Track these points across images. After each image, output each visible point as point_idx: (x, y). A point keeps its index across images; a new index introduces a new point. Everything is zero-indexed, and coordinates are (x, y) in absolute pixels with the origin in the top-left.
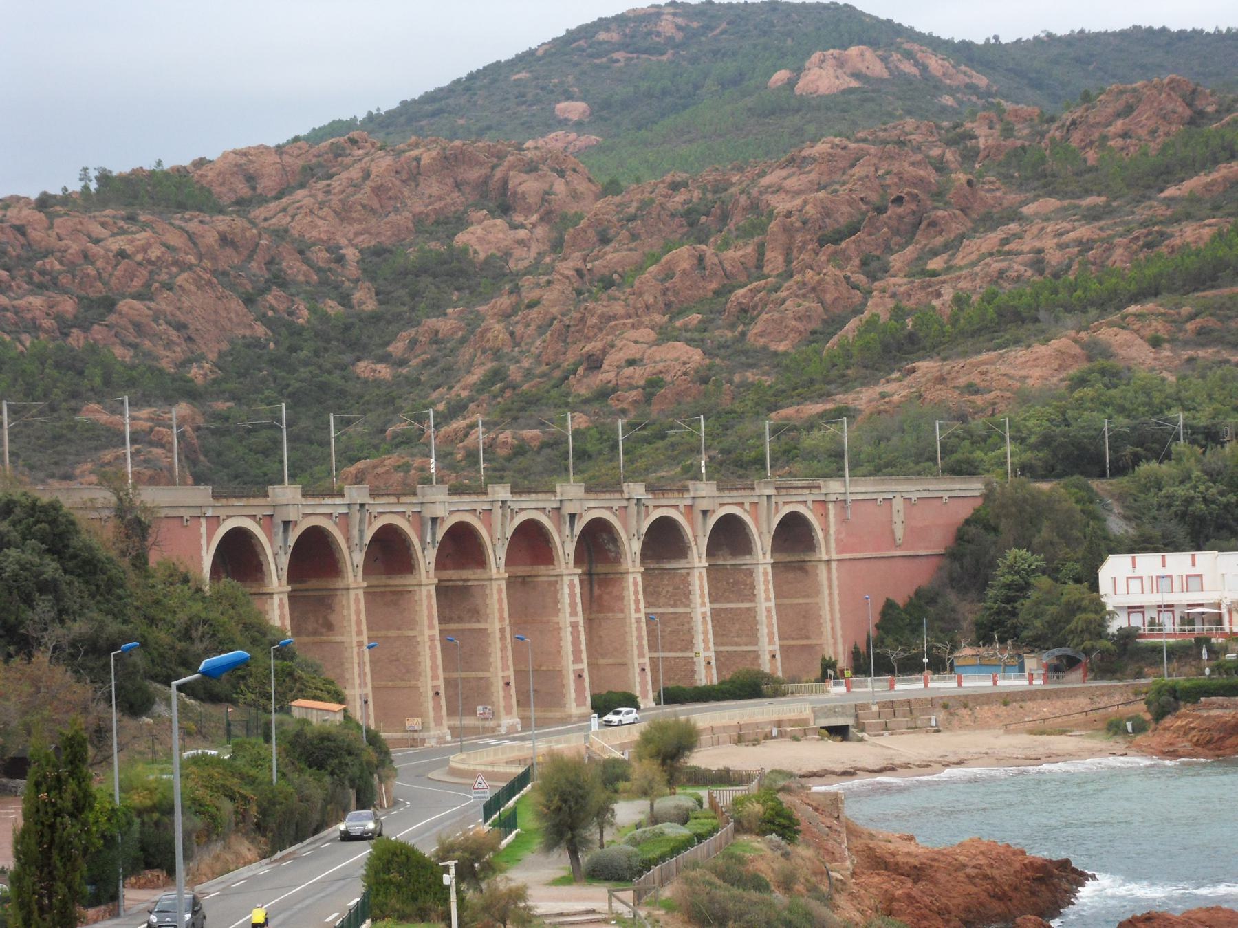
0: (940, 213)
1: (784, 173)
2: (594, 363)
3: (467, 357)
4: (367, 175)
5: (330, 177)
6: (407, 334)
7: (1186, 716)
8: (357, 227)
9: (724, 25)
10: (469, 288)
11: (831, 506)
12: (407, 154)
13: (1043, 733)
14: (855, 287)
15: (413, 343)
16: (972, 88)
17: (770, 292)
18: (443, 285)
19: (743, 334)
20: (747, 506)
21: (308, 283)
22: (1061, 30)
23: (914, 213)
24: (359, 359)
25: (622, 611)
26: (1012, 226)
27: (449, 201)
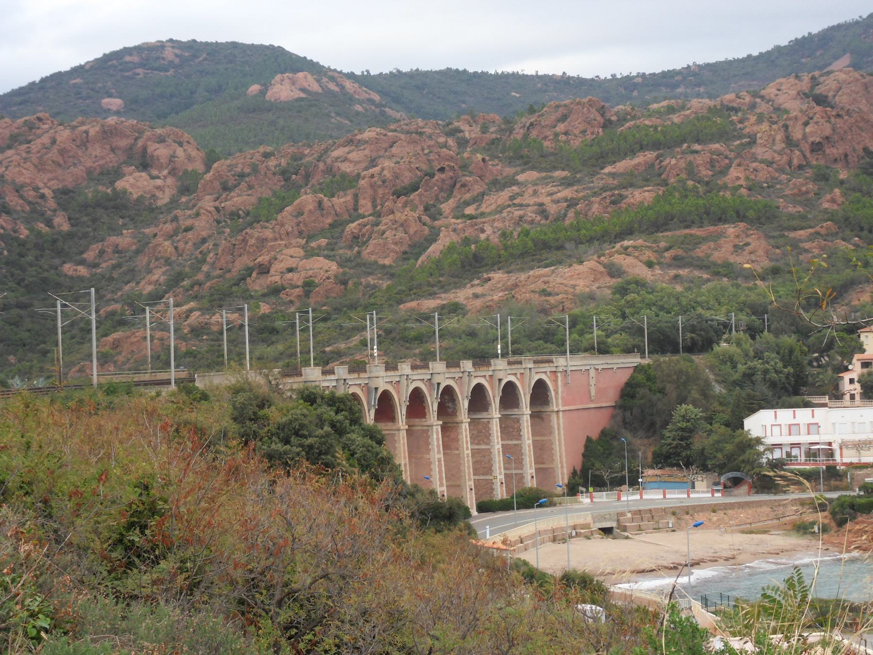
0: (467, 178)
1: (347, 149)
2: (264, 270)
3: (144, 263)
4: (54, 141)
5: (29, 142)
6: (96, 247)
7: (863, 522)
8: (49, 175)
9: (205, 55)
10: (129, 216)
11: (559, 374)
12: (80, 128)
13: (751, 532)
14: (424, 224)
15: (102, 252)
16: (371, 101)
17: (373, 225)
18: (112, 215)
19: (359, 253)
20: (518, 376)
21: (23, 211)
22: (405, 69)
23: (452, 178)
24: (64, 262)
25: (458, 449)
26: (514, 188)
27: (108, 160)
